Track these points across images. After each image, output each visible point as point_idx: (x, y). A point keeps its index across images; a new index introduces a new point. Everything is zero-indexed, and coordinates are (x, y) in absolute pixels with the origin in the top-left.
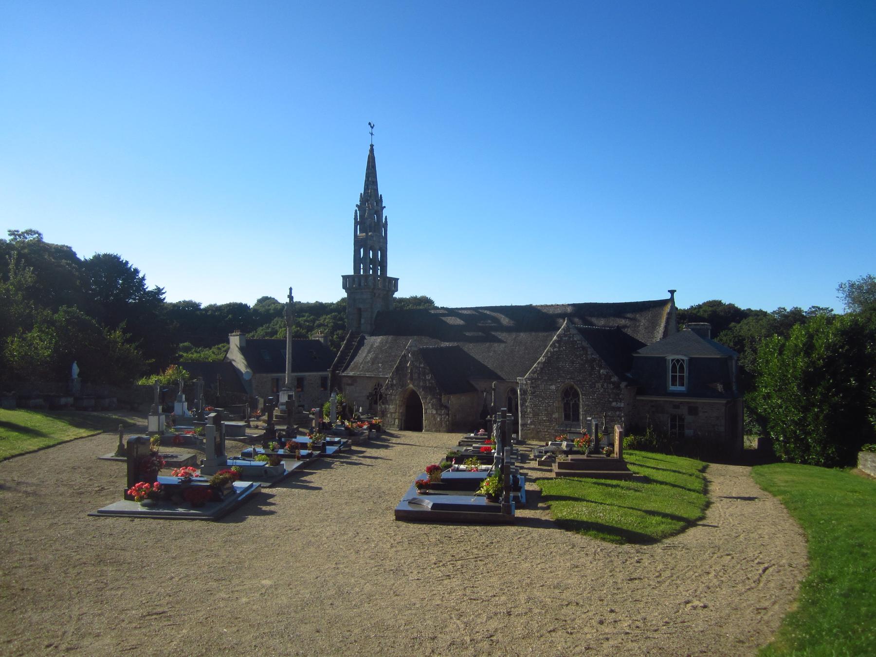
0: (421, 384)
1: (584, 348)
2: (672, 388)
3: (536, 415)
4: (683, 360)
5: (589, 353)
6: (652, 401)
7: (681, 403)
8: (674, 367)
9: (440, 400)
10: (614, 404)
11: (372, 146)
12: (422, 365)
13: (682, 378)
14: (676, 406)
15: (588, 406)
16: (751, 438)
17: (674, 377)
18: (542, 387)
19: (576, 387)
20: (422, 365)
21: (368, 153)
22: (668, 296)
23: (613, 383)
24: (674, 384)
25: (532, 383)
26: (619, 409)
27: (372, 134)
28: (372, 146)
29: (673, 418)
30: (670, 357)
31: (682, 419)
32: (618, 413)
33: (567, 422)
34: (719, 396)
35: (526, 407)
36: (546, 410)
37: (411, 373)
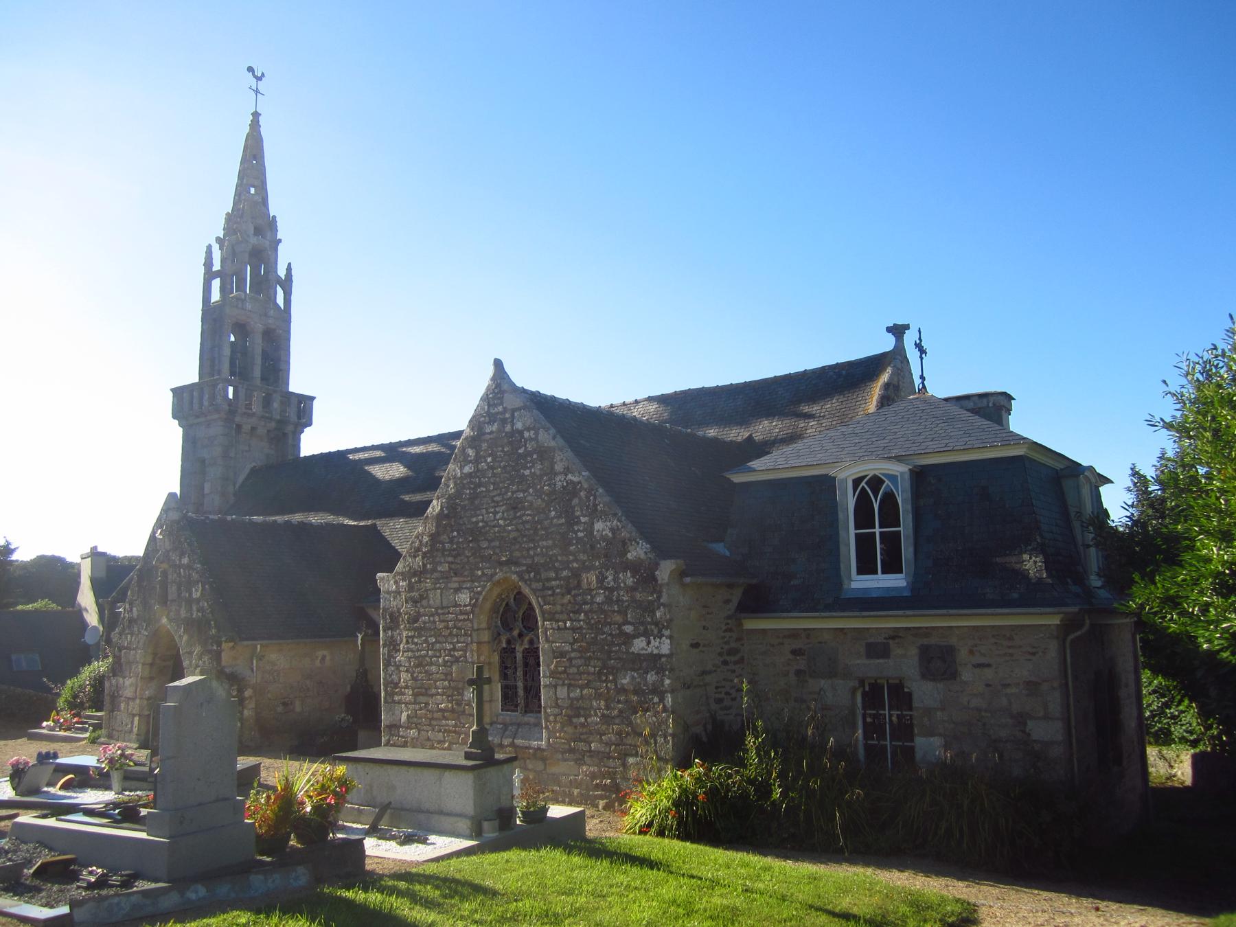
0: (183, 613)
1: (544, 454)
2: (860, 583)
3: (422, 691)
4: (893, 478)
5: (558, 467)
6: (794, 634)
7: (895, 635)
8: (863, 505)
9: (217, 656)
10: (639, 644)
11: (256, 115)
12: (185, 561)
13: (892, 542)
14: (878, 649)
15: (562, 654)
16: (1169, 752)
17: (864, 543)
18: (435, 598)
19: (526, 591)
20: (185, 561)
21: (247, 129)
22: (887, 343)
23: (634, 567)
24: (866, 567)
25: (411, 588)
26: (654, 661)
27: (257, 92)
28: (256, 115)
29: (873, 695)
30: (846, 473)
31: (901, 696)
32: (651, 677)
33: (510, 716)
34: (1031, 595)
35: (398, 666)
36: (447, 675)
37: (164, 585)
